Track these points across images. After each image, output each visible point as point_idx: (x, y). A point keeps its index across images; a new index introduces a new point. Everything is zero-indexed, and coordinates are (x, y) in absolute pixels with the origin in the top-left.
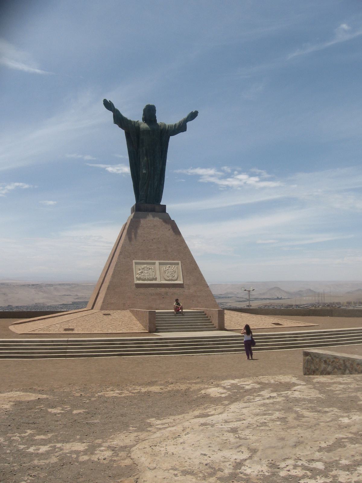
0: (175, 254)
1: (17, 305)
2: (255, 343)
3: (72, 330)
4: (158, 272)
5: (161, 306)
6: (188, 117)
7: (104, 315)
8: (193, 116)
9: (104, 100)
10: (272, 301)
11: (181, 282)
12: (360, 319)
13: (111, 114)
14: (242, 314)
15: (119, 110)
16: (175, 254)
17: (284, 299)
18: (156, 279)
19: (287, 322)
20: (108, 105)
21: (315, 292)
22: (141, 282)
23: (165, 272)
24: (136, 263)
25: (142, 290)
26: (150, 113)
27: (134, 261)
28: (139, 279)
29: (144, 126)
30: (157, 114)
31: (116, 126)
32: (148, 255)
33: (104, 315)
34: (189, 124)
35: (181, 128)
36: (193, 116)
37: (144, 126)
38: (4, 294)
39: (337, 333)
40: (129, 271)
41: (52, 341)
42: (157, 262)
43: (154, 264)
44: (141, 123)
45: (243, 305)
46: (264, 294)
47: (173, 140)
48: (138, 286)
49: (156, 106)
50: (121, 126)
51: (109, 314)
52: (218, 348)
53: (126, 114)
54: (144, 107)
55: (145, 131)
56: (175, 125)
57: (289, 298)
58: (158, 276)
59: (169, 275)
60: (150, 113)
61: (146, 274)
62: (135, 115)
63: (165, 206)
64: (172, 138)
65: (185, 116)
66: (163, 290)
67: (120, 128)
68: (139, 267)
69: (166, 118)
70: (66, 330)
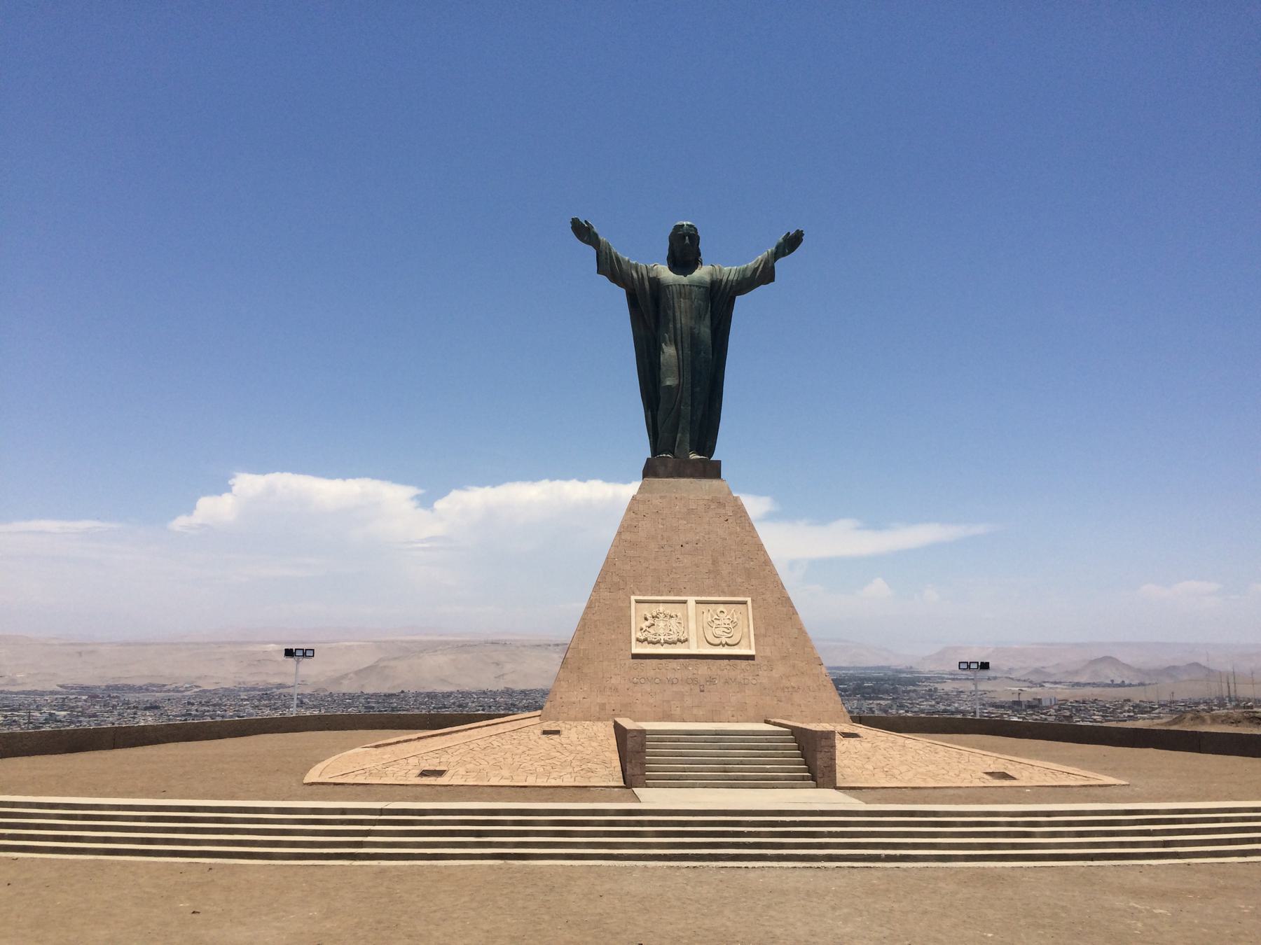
0: (739, 580)
1: (523, 688)
3: (440, 773)
7: (545, 732)
8: (792, 243)
10: (1097, 691)
11: (752, 652)
13: (591, 251)
14: (908, 742)
16: (739, 580)
17: (1130, 685)
18: (698, 602)
19: (1040, 769)
20: (583, 231)
21: (1210, 671)
24: (637, 602)
26: (684, 250)
27: (633, 598)
31: (604, 279)
32: (670, 585)
33: (545, 732)
34: (780, 265)
35: (765, 275)
36: (792, 243)
38: (497, 664)
39: (1174, 817)
41: (343, 811)
42: (691, 600)
46: (1076, 672)
47: (743, 305)
51: (557, 732)
53: (626, 253)
54: (196, 513)
57: (1141, 684)
59: (718, 632)
60: (684, 250)
63: (719, 462)
66: (703, 668)
68: (647, 610)
70: (424, 774)
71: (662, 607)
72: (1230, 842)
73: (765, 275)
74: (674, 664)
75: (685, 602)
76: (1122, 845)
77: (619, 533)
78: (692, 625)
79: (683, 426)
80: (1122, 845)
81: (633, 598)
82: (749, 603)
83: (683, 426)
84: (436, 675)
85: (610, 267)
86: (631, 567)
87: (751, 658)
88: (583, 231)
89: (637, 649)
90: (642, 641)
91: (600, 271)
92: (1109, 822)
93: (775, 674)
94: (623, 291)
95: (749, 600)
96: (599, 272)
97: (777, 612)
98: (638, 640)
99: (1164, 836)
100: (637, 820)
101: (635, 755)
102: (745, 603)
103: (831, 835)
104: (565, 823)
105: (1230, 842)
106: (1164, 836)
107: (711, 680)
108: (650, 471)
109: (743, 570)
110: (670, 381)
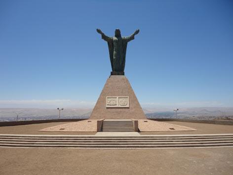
4: (117, 102)
5: (118, 118)
8: (137, 32)
12: (2, 121)
18: (116, 105)
19: (179, 127)
20: (99, 31)
22: (109, 106)
23: (121, 102)
25: (109, 110)
26: (118, 34)
28: (108, 105)
31: (103, 40)
34: (135, 36)
35: (132, 38)
36: (137, 32)
37: (115, 38)
40: (104, 101)
42: (118, 97)
45: (150, 117)
47: (129, 43)
48: (108, 108)
50: (105, 40)
52: (119, 144)
55: (116, 41)
58: (117, 103)
60: (118, 34)
61: (112, 103)
64: (128, 43)
66: (119, 110)
69: (124, 36)
72: (216, 143)
73: (132, 38)
76: (192, 144)
78: (117, 102)
79: (118, 68)
80: (192, 144)
83: (118, 68)
84: (76, 116)
87: (128, 108)
88: (99, 31)
89: (108, 106)
92: (190, 138)
93: (133, 111)
94: (107, 42)
97: (134, 100)
99: (202, 142)
100: (101, 139)
103: (130, 142)
104: (87, 140)
105: (216, 143)
106: (202, 142)
107: (121, 112)
108: (112, 74)
109: (129, 92)
110: (114, 58)
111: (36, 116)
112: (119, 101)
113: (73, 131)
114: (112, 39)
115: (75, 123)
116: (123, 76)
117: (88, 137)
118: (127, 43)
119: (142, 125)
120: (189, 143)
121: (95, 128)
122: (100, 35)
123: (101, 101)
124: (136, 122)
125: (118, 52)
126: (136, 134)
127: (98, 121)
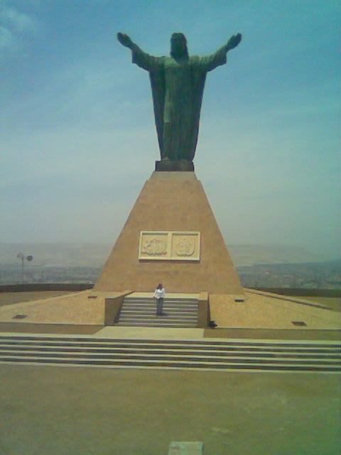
2: (198, 308)
4: (169, 245)
6: (228, 44)
7: (236, 301)
8: (235, 41)
9: (175, 35)
11: (198, 259)
15: (121, 45)
20: (124, 39)
24: (143, 234)
26: (179, 44)
27: (141, 232)
29: (170, 62)
30: (189, 46)
31: (135, 65)
32: (160, 224)
33: (236, 301)
35: (220, 59)
36: (235, 41)
37: (170, 62)
40: (134, 244)
42: (170, 233)
43: (167, 234)
44: (168, 59)
47: (211, 76)
49: (184, 34)
51: (95, 297)
54: (169, 37)
55: (173, 70)
56: (211, 56)
60: (179, 44)
61: (154, 248)
62: (160, 50)
65: (225, 43)
66: (173, 267)
67: (142, 69)
69: (199, 49)
71: (155, 237)
73: (220, 59)
74: (159, 265)
75: (167, 234)
77: (138, 200)
78: (169, 245)
79: (178, 145)
81: (141, 232)
82: (199, 235)
83: (178, 145)
85: (140, 59)
86: (145, 215)
88: (124, 39)
89: (143, 258)
90: (145, 253)
91: (134, 61)
94: (147, 73)
95: (199, 233)
96: (133, 62)
98: (142, 253)
101: (115, 313)
102: (197, 235)
107: (177, 273)
108: (159, 167)
109: (199, 216)
111: (35, 279)
112: (176, 245)
113: (47, 322)
114: (163, 65)
115: (72, 295)
116: (190, 173)
117: (75, 340)
118: (203, 77)
119: (226, 311)
120: (127, 295)
121: (100, 318)
122: (128, 53)
123: (127, 240)
124: (204, 307)
125: (179, 92)
126: (197, 334)
127: (108, 301)
